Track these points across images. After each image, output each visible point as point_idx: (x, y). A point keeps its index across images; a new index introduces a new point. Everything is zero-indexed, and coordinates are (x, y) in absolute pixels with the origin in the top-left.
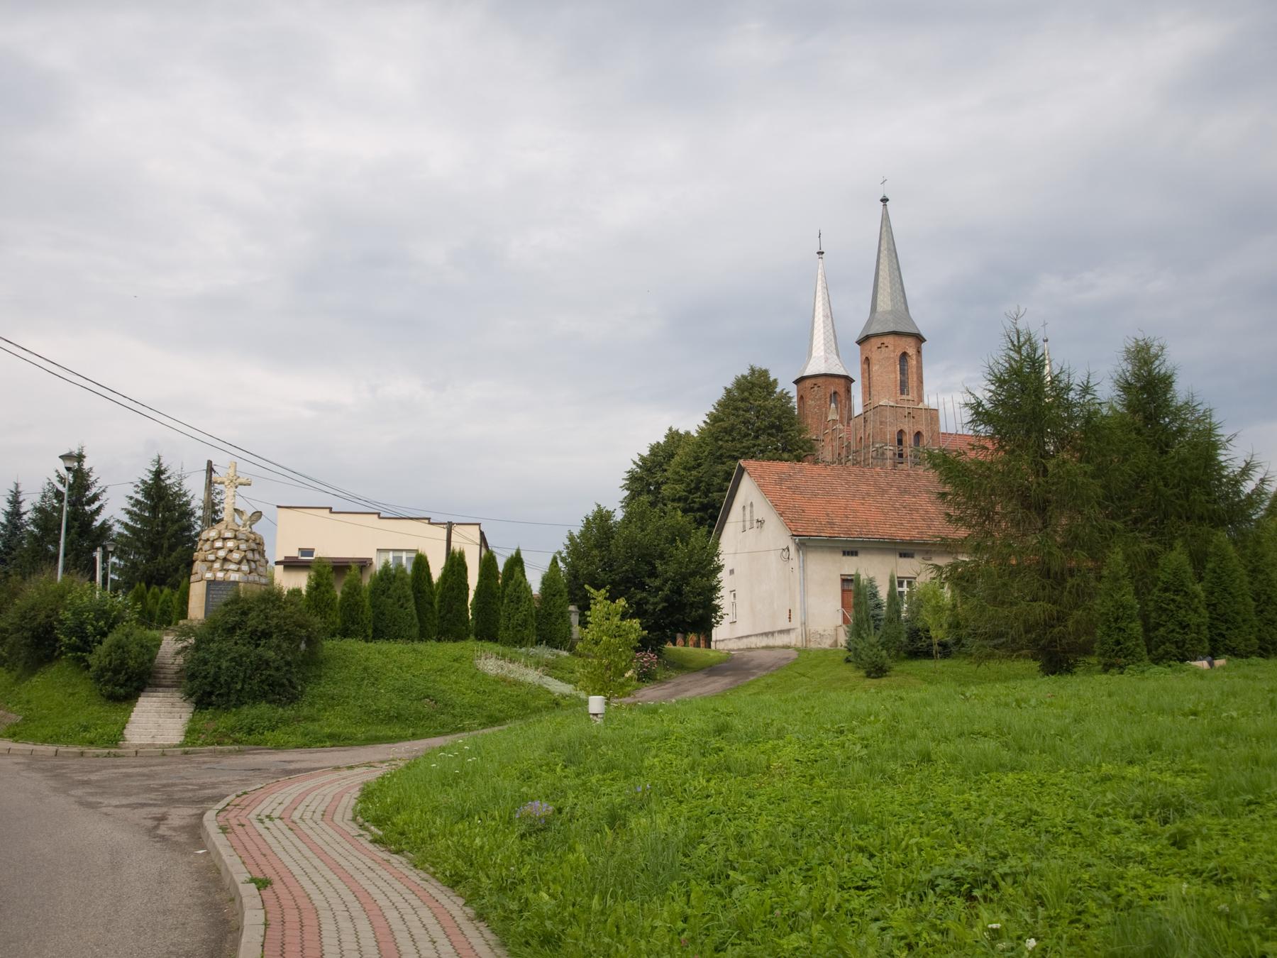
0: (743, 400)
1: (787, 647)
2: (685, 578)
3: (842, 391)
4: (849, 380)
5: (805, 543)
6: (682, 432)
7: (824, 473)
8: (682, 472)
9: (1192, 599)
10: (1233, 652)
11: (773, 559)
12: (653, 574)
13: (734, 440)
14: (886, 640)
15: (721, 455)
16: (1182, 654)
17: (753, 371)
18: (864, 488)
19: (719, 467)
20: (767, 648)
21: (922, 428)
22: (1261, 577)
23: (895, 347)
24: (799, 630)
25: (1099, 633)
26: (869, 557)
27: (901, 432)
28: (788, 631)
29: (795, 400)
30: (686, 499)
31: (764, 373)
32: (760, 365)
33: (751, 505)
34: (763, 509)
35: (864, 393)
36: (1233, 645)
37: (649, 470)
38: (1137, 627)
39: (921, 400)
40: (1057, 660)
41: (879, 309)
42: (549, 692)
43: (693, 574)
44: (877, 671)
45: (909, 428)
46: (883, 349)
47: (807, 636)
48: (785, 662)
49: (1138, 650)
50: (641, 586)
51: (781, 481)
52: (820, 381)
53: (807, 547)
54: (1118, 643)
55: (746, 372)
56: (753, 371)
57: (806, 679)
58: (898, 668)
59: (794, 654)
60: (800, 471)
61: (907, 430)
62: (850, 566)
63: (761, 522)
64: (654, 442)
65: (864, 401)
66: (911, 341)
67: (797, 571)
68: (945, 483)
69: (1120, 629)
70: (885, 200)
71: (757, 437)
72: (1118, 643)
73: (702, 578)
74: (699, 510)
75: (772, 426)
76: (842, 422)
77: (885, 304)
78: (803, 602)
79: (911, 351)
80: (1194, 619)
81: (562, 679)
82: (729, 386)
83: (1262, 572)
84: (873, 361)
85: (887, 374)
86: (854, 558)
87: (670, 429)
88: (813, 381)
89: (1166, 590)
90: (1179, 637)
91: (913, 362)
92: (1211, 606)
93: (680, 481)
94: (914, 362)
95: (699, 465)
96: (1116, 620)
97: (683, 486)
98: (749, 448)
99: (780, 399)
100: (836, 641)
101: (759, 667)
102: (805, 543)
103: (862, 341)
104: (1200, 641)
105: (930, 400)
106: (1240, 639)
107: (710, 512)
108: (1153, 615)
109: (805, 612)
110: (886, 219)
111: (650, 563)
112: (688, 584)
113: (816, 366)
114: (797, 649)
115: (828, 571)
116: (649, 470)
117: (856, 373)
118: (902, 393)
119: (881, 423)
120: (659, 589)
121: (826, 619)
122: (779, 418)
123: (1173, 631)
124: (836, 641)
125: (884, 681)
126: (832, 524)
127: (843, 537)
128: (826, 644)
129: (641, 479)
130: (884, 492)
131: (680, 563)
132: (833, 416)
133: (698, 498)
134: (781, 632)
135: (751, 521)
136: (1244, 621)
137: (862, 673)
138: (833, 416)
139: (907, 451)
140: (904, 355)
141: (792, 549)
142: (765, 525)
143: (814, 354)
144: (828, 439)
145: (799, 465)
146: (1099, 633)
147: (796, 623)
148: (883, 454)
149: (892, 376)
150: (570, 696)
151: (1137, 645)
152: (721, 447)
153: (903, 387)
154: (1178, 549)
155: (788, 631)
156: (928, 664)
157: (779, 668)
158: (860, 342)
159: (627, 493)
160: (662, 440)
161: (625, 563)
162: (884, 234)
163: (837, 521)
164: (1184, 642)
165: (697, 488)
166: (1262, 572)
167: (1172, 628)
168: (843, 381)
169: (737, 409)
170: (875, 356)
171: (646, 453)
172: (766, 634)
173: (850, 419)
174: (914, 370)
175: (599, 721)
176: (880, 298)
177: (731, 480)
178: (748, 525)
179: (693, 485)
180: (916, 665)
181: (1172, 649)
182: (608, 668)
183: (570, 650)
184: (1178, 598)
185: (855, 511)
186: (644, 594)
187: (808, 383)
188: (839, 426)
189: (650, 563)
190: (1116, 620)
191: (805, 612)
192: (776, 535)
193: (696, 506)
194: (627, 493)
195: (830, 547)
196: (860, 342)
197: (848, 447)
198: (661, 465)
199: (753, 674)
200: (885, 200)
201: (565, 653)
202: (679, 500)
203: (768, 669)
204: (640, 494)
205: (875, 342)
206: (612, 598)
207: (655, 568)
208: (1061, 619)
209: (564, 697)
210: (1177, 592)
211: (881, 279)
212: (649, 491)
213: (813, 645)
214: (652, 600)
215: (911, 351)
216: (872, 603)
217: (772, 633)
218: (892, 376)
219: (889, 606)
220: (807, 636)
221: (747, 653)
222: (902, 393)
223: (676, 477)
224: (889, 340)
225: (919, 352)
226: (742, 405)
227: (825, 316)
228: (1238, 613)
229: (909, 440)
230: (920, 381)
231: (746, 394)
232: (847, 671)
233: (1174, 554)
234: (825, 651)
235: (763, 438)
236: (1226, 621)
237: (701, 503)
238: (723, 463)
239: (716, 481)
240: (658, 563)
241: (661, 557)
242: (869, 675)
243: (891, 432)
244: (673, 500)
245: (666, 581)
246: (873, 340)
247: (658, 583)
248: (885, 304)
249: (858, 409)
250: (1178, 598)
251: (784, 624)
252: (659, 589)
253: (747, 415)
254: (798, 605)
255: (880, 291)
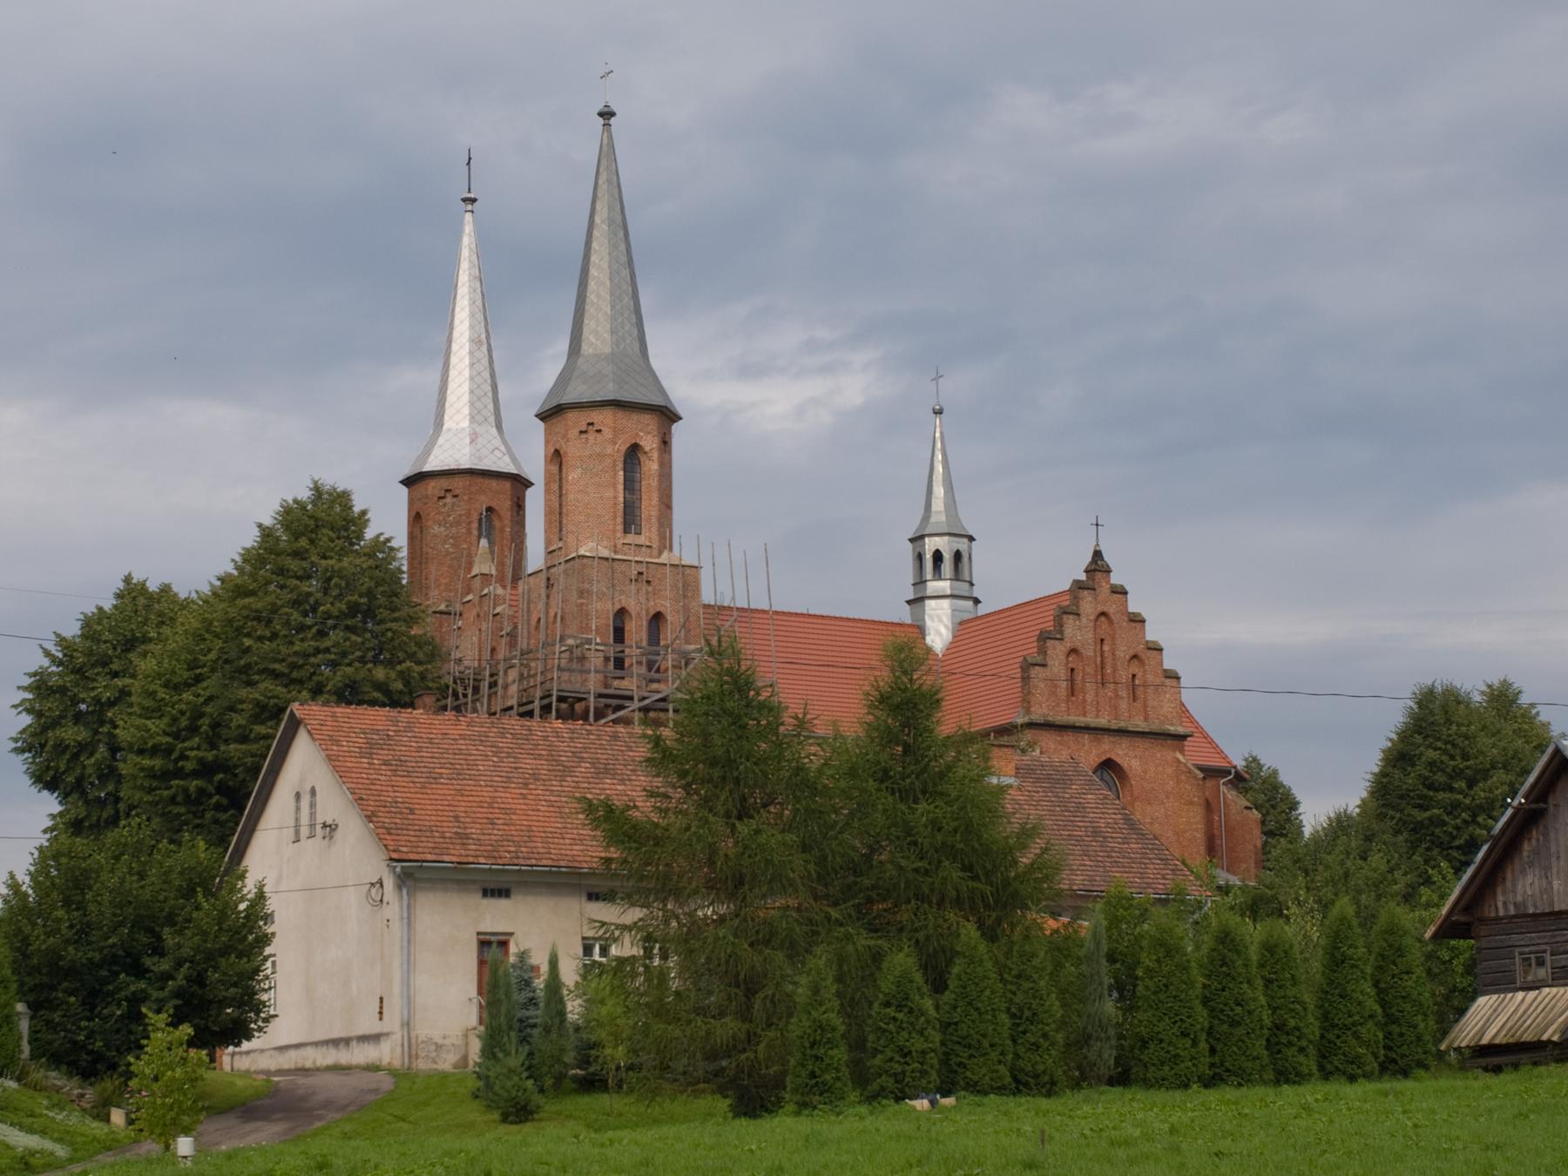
0: (298, 554)
1: (373, 1068)
2: (211, 958)
3: (504, 506)
4: (520, 483)
5: (414, 875)
6: (153, 586)
7: (454, 732)
8: (162, 694)
9: (917, 1018)
10: (976, 1088)
11: (353, 900)
12: (158, 950)
13: (274, 636)
14: (534, 1056)
15: (248, 666)
16: (902, 1091)
17: (317, 489)
18: (528, 763)
19: (243, 693)
20: (336, 1068)
21: (666, 605)
22: (1026, 985)
23: (614, 433)
24: (397, 1037)
25: (793, 1062)
26: (530, 899)
27: (621, 613)
28: (375, 1038)
29: (404, 553)
30: (168, 751)
31: (343, 498)
32: (335, 478)
33: (313, 792)
34: (334, 804)
35: (548, 522)
36: (975, 1078)
37: (79, 671)
38: (840, 1054)
39: (666, 542)
40: (754, 1099)
41: (586, 349)
42: (8, 1147)
43: (225, 952)
44: (519, 1112)
45: (638, 604)
46: (591, 436)
47: (411, 1048)
48: (371, 1097)
49: (839, 1084)
50: (140, 972)
51: (369, 749)
52: (458, 484)
53: (416, 880)
54: (813, 1075)
55: (305, 494)
56: (317, 489)
57: (406, 1126)
58: (550, 1106)
59: (386, 1083)
60: (409, 728)
61: (633, 607)
62: (496, 916)
63: (330, 828)
64: (90, 609)
65: (548, 542)
66: (649, 421)
67: (396, 926)
68: (608, 846)
69: (816, 1057)
70: (607, 114)
71: (322, 634)
72: (813, 1075)
73: (239, 957)
74: (195, 774)
75: (354, 609)
76: (501, 579)
77: (598, 338)
78: (407, 984)
79: (649, 443)
80: (918, 1044)
81: (21, 1127)
82: (268, 521)
83: (1029, 978)
84: (569, 461)
85: (595, 492)
86: (503, 903)
87: (128, 579)
88: (444, 483)
89: (887, 1004)
90: (898, 1068)
91: (651, 466)
92: (945, 1026)
93: (154, 712)
94: (655, 466)
95: (198, 679)
96: (812, 1045)
97: (163, 723)
98: (306, 655)
99: (371, 555)
100: (465, 1058)
101: (328, 1104)
102: (414, 875)
103: (550, 415)
104: (924, 1073)
105: (684, 551)
106: (984, 1070)
107: (226, 797)
108: (871, 1037)
109: (409, 1002)
110: (607, 153)
111: (151, 931)
112: (216, 968)
113: (452, 451)
114: (392, 1072)
115: (452, 926)
116: (79, 671)
117: (534, 466)
118: (626, 531)
119: (581, 593)
120: (167, 976)
121: (446, 1013)
122: (369, 593)
123: (891, 1060)
124: (465, 1058)
125: (528, 1127)
126: (463, 837)
127: (484, 863)
128: (447, 1062)
129: (62, 690)
130: (565, 772)
131: (204, 933)
132: (483, 565)
133: (195, 751)
134: (364, 1039)
135: (312, 826)
136: (992, 1045)
137: (496, 1116)
138: (483, 565)
139: (632, 653)
140: (634, 450)
141: (389, 884)
142: (338, 834)
143: (448, 423)
144: (471, 615)
145: (405, 715)
146: (793, 1062)
147: (392, 1022)
148: (583, 659)
149: (609, 494)
150: (41, 1152)
151: (838, 1079)
152: (248, 650)
153: (631, 519)
154: (906, 950)
155: (375, 1038)
156: (603, 1101)
157: (362, 1107)
158: (544, 416)
159: (26, 720)
160: (108, 604)
161: (114, 930)
162: (603, 187)
163: (473, 830)
164: (904, 1073)
165: (193, 729)
166: (1029, 978)
167: (890, 1054)
168: (507, 485)
169: (281, 571)
170: (573, 450)
171: (72, 630)
172: (335, 1043)
173: (516, 578)
174: (654, 483)
175: (189, 1163)
176: (589, 324)
177: (269, 735)
178: (304, 831)
179: (184, 722)
180: (586, 1101)
181: (889, 1082)
182: (171, 1108)
183: (19, 1080)
184: (900, 1016)
185: (507, 811)
186: (142, 985)
187: (433, 487)
188: (496, 589)
189: (151, 931)
190: (812, 1045)
191: (409, 1002)
192: (357, 856)
193: (189, 766)
194: (26, 720)
195: (458, 881)
196: (544, 416)
197: (512, 635)
198: (104, 662)
199: (319, 1118)
200: (607, 114)
201: (12, 1084)
202: (155, 751)
203: (343, 1108)
204: (55, 723)
205: (576, 420)
206: (175, 1023)
207: (159, 938)
208: (751, 1039)
209: (33, 1153)
210: (900, 1008)
211: (592, 285)
212: (78, 718)
213: (422, 1065)
214: (155, 994)
215: (649, 443)
216: (521, 997)
217: (347, 1041)
218: (609, 494)
219: (548, 1004)
220: (411, 1048)
221: (301, 1081)
222: (626, 531)
223: (148, 703)
224: (603, 418)
225: (665, 443)
226: (294, 565)
227: (476, 342)
228: (984, 1036)
229: (636, 631)
230: (666, 504)
231: (303, 542)
232: (473, 1112)
233: (901, 955)
234: (444, 1076)
235: (335, 636)
236: (969, 1046)
237: (201, 761)
238: (250, 683)
239: (238, 720)
240: (166, 933)
241: (170, 920)
242: (505, 1118)
243: (601, 611)
244: (141, 752)
245: (179, 964)
246: (571, 416)
247: (165, 965)
248: (598, 338)
249: (535, 555)
250: (900, 1016)
251: (368, 1025)
252: (167, 976)
253: (305, 587)
254: (397, 988)
255: (590, 310)
